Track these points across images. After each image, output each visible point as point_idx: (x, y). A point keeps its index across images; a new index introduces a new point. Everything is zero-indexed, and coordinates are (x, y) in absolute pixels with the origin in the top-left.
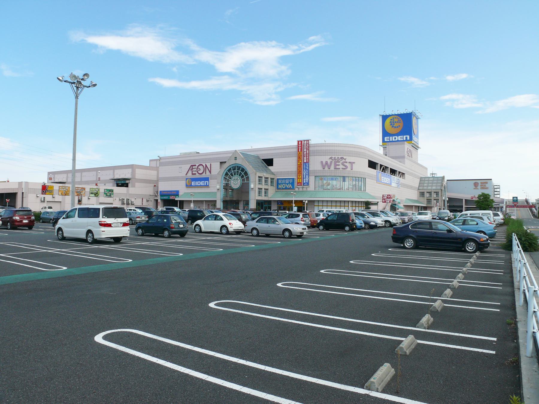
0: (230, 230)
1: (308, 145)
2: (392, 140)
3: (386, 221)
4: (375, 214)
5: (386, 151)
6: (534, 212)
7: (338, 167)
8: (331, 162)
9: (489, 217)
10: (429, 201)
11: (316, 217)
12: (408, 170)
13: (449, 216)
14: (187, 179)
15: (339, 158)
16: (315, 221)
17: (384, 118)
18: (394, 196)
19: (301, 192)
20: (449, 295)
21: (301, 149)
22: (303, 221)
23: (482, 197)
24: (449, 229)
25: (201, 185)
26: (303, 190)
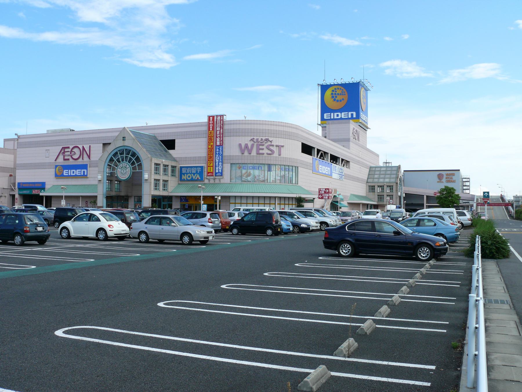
0: (110, 234)
1: (222, 122)
2: (334, 117)
3: (322, 223)
4: (307, 214)
5: (326, 132)
6: (511, 211)
7: (261, 152)
9: (452, 217)
10: (381, 197)
11: (229, 217)
12: (354, 157)
13: (404, 217)
14: (56, 166)
15: (263, 140)
16: (227, 223)
17: (324, 88)
18: (335, 190)
19: (213, 185)
20: (386, 313)
21: (213, 127)
22: (211, 222)
23: (445, 192)
24: (397, 230)
25: (76, 175)
26: (215, 182)
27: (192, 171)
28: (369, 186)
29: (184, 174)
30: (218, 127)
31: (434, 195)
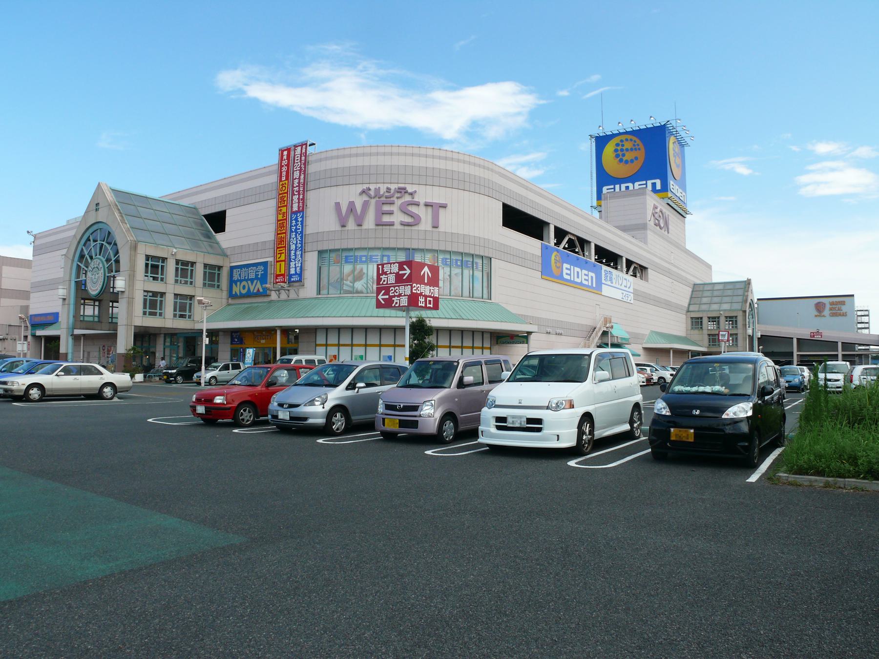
1: (303, 158)
7: (386, 219)
8: (366, 205)
15: (392, 191)
17: (601, 142)
21: (287, 172)
27: (248, 274)
28: (691, 318)
29: (236, 282)
30: (296, 171)
31: (811, 337)
